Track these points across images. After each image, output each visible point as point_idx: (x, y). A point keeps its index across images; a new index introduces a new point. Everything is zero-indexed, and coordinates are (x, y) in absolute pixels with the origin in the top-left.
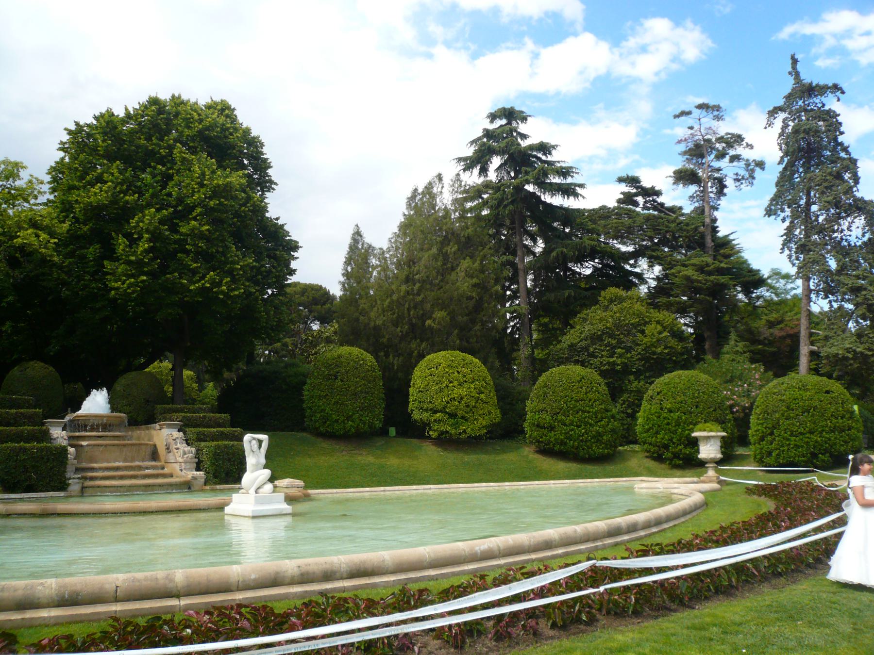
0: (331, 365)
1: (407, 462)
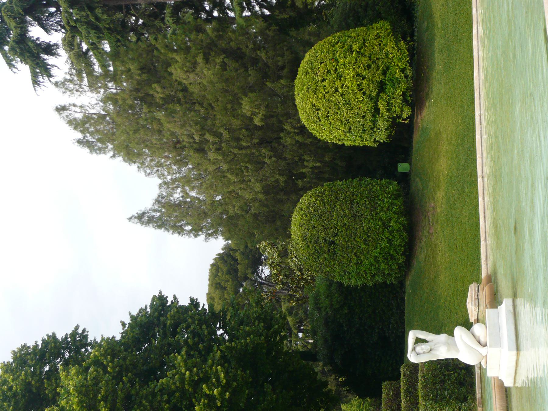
0: (316, 249)
1: (444, 148)
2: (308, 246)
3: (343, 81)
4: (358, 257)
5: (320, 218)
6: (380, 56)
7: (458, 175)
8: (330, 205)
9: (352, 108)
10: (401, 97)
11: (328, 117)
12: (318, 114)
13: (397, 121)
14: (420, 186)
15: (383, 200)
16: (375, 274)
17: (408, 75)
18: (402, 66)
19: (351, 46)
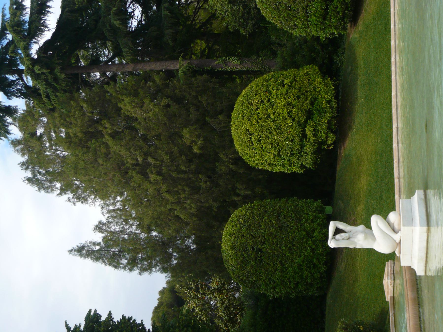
0: (244, 257)
2: (237, 255)
3: (275, 109)
4: (283, 265)
5: (249, 228)
6: (309, 90)
7: (376, 187)
9: (282, 132)
10: (326, 124)
11: (260, 141)
12: (251, 138)
13: (323, 148)
15: (308, 214)
16: (298, 283)
17: (333, 106)
18: (328, 98)
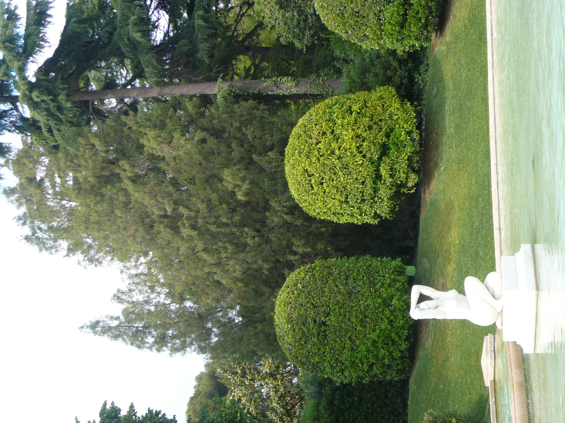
1: (456, 215)
3: (340, 143)
4: (353, 342)
5: (309, 295)
6: (383, 118)
7: (471, 240)
8: (322, 280)
9: (350, 172)
11: (322, 184)
12: (310, 181)
13: (402, 192)
14: (427, 266)
16: (373, 364)
17: (415, 139)
18: (407, 128)
19: (350, 107)
